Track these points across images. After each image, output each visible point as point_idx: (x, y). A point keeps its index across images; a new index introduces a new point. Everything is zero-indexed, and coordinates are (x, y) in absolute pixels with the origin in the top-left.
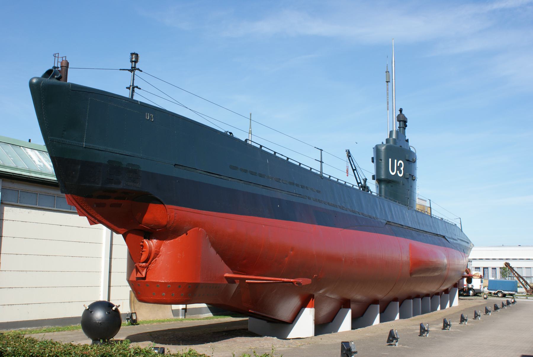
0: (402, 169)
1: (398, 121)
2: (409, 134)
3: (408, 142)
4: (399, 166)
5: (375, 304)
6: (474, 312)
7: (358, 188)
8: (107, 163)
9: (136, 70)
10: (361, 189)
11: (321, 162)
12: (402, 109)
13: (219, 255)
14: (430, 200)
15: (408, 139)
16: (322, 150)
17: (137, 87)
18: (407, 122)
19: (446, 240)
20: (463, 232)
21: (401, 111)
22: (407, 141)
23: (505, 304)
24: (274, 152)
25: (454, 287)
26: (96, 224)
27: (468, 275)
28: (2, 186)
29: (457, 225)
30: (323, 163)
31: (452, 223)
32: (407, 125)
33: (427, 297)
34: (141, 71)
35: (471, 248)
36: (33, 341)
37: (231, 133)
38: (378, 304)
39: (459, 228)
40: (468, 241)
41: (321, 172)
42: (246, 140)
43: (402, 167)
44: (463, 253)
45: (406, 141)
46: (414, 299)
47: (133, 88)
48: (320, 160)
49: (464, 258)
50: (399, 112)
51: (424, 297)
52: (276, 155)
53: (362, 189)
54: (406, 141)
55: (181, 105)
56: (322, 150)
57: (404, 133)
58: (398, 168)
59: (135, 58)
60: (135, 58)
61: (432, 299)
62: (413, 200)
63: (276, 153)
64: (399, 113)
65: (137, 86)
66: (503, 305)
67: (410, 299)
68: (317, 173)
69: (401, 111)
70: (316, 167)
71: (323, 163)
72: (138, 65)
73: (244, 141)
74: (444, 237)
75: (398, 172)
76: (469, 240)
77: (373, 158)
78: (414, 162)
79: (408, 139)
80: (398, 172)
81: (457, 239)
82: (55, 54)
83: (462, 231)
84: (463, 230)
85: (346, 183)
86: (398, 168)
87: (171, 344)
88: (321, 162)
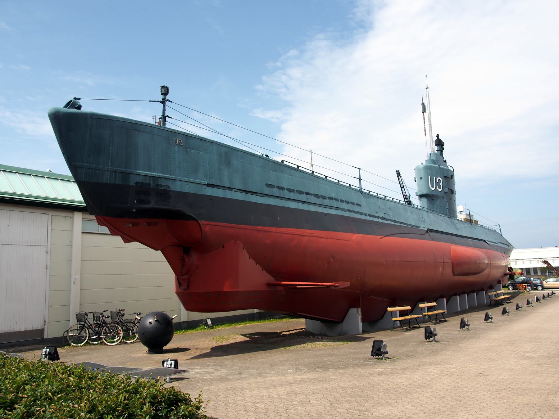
0: (441, 184)
1: (436, 145)
2: (446, 154)
3: (446, 162)
4: (438, 182)
5: (422, 301)
6: (516, 305)
7: (404, 203)
8: (135, 185)
9: (166, 101)
10: (407, 203)
11: (360, 179)
12: (438, 135)
13: (260, 265)
14: (469, 210)
15: (446, 160)
16: (360, 169)
17: (168, 116)
18: (444, 146)
19: (486, 243)
20: (503, 236)
21: (438, 136)
22: (445, 161)
23: (546, 296)
24: (297, 166)
25: (498, 283)
26: (132, 242)
27: (511, 273)
28: (82, 218)
29: (497, 231)
30: (362, 180)
31: (492, 229)
32: (444, 148)
33: (454, 296)
34: (171, 102)
35: (511, 249)
36: (257, 322)
37: (267, 156)
38: (425, 301)
39: (499, 234)
40: (508, 244)
41: (361, 188)
42: (282, 161)
43: (440, 183)
44: (504, 254)
45: (444, 161)
46: (460, 296)
47: (164, 118)
48: (359, 178)
49: (505, 259)
50: (436, 137)
51: (470, 293)
52: (284, 163)
53: (408, 203)
54: (444, 161)
55: (235, 140)
56: (360, 169)
57: (442, 155)
58: (438, 183)
59: (165, 91)
60: (165, 91)
61: (469, 296)
62: (453, 210)
63: (314, 173)
64: (436, 138)
65: (168, 115)
66: (544, 297)
67: (474, 292)
68: (357, 189)
69: (438, 136)
70: (355, 184)
71: (362, 180)
72: (168, 97)
73: (280, 161)
74: (485, 241)
75: (437, 187)
76: (510, 243)
77: (415, 178)
78: (452, 177)
79: (446, 160)
80: (437, 187)
81: (497, 242)
82: (153, 117)
83: (502, 236)
84: (503, 235)
85: (386, 197)
86: (438, 183)
87: (426, 302)
88: (360, 179)
